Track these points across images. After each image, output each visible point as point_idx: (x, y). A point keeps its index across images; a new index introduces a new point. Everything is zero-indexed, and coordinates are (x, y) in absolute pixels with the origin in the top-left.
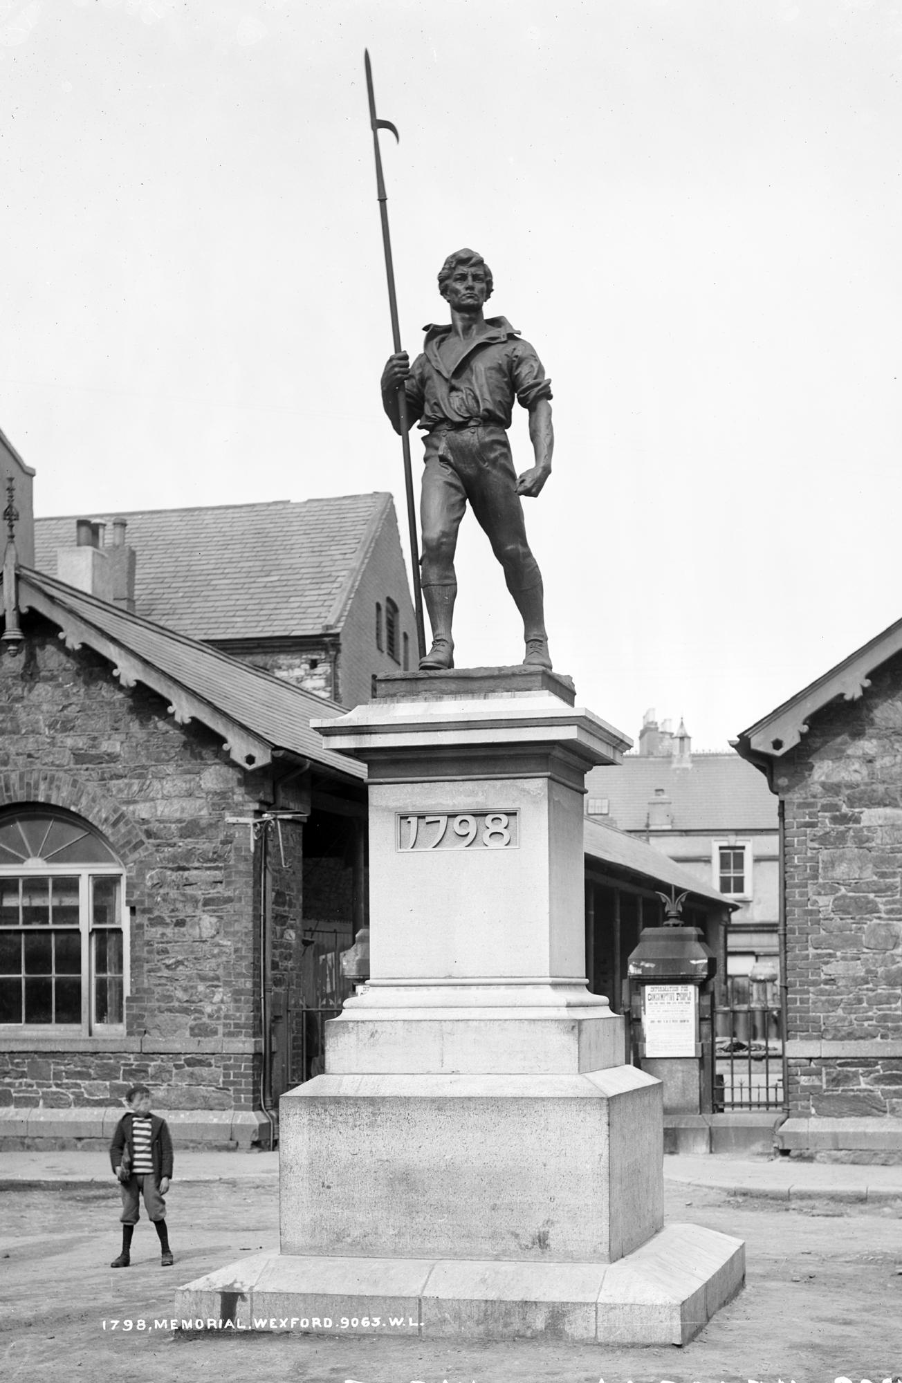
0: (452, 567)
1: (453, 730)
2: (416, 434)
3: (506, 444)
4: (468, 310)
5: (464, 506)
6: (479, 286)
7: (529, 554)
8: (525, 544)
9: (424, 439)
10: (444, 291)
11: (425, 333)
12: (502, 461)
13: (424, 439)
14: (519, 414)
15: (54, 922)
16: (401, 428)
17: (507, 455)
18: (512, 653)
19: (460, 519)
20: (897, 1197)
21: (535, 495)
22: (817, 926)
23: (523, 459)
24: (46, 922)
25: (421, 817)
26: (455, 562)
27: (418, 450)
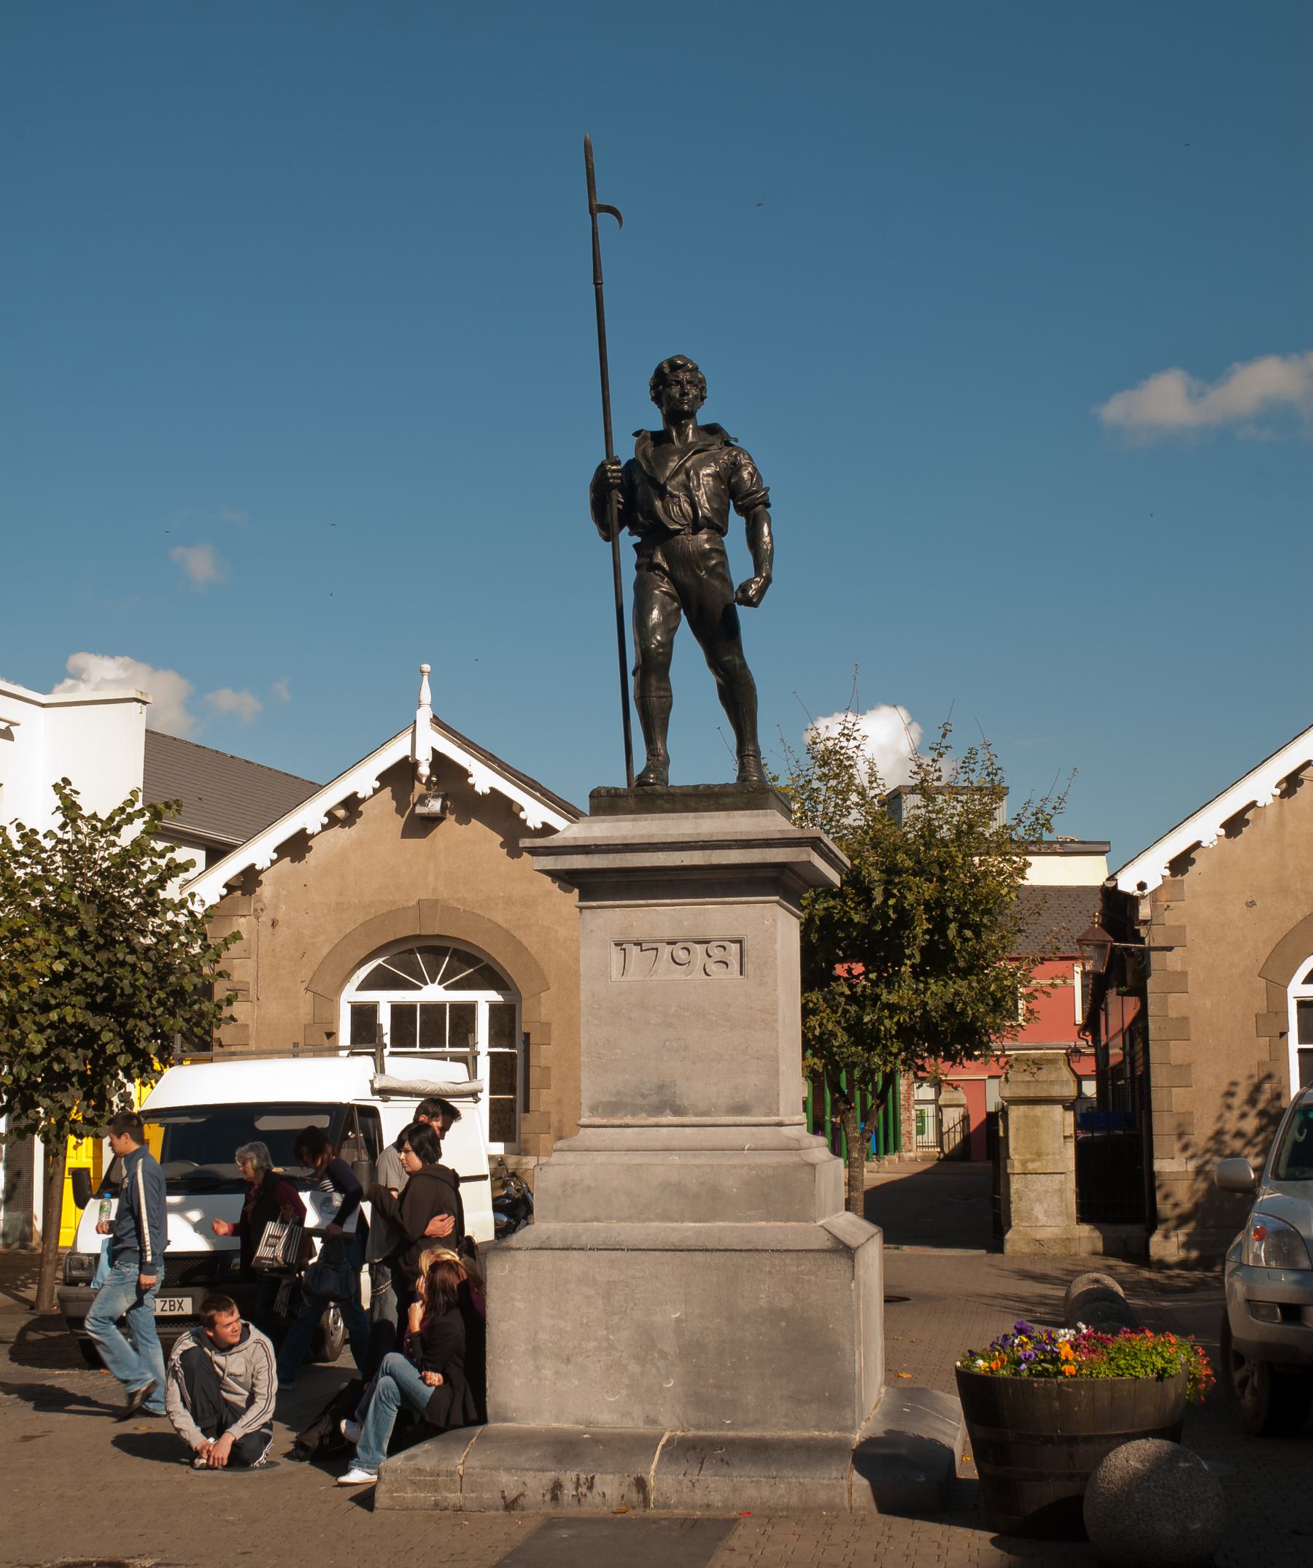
0: (667, 679)
1: (291, 776)
2: (627, 540)
3: (722, 553)
4: (677, 416)
5: (679, 617)
6: (694, 392)
7: (744, 666)
8: (742, 657)
9: (636, 546)
10: (657, 399)
11: (636, 439)
12: (720, 570)
13: (636, 546)
14: (737, 523)
15: (451, 1045)
16: (609, 534)
17: (724, 563)
18: (724, 771)
19: (675, 629)
20: (9, 1389)
21: (755, 605)
22: (1036, 1129)
23: (740, 567)
24: (445, 1047)
25: (638, 944)
26: (671, 674)
27: (629, 558)
